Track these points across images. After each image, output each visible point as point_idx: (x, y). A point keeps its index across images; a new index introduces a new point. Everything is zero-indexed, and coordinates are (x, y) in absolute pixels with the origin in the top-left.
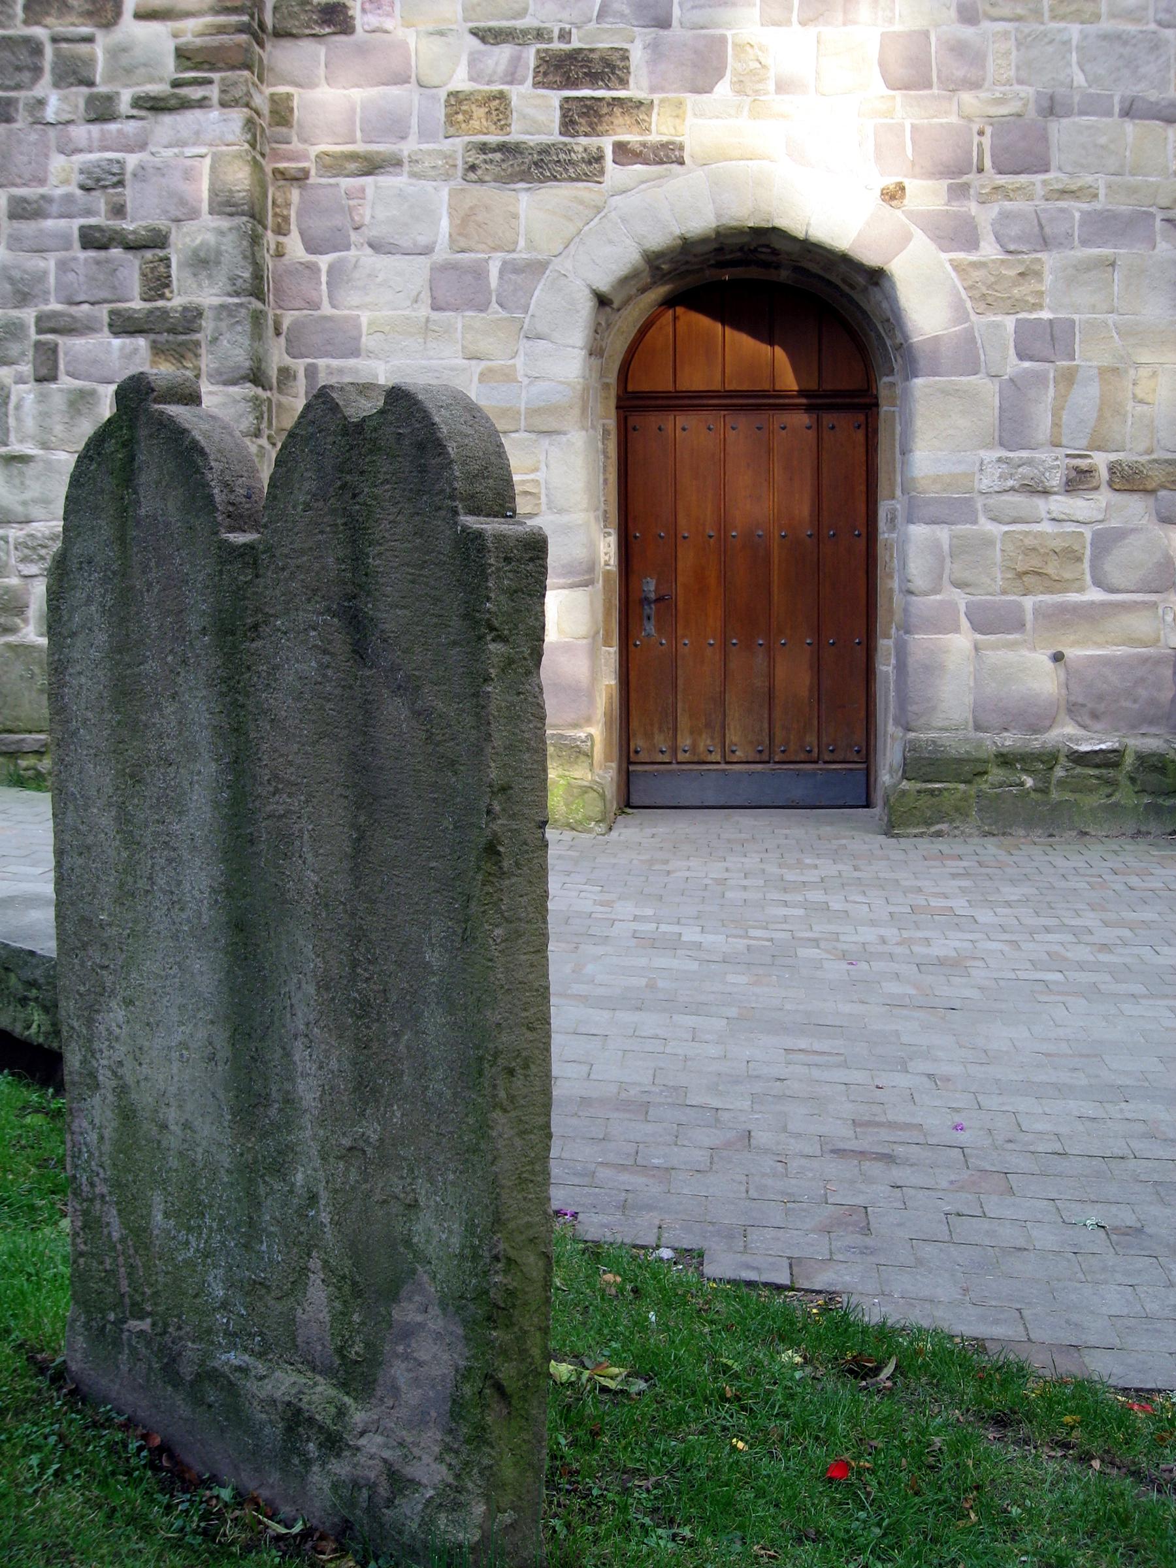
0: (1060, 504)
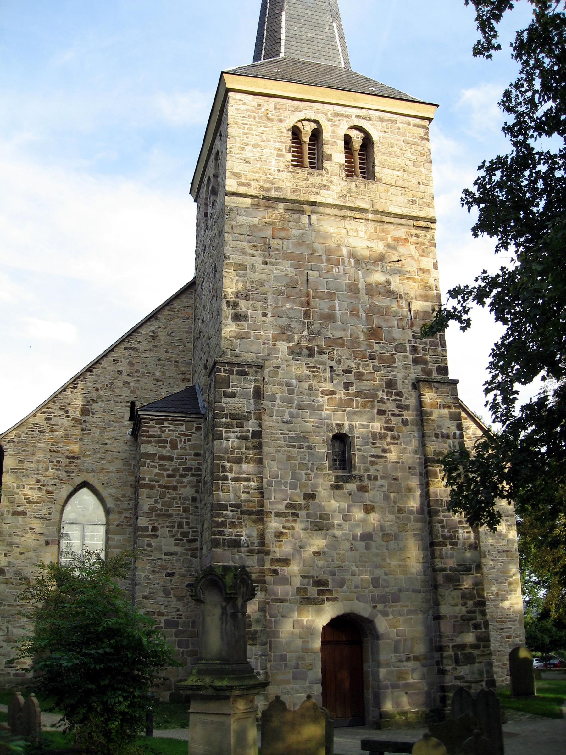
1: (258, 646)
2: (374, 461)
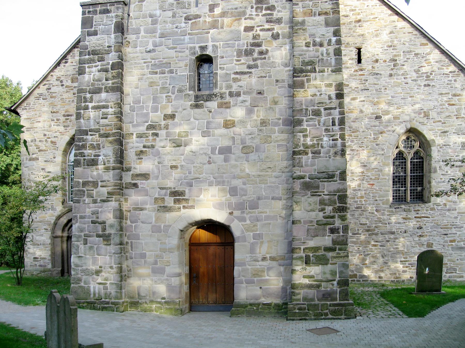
0: (261, 263)
1: (112, 246)
2: (237, 78)
